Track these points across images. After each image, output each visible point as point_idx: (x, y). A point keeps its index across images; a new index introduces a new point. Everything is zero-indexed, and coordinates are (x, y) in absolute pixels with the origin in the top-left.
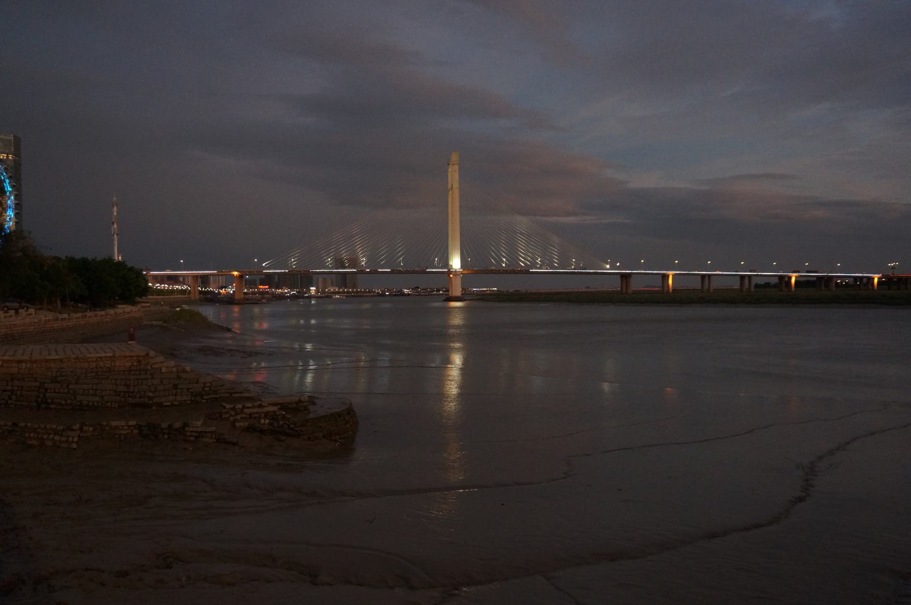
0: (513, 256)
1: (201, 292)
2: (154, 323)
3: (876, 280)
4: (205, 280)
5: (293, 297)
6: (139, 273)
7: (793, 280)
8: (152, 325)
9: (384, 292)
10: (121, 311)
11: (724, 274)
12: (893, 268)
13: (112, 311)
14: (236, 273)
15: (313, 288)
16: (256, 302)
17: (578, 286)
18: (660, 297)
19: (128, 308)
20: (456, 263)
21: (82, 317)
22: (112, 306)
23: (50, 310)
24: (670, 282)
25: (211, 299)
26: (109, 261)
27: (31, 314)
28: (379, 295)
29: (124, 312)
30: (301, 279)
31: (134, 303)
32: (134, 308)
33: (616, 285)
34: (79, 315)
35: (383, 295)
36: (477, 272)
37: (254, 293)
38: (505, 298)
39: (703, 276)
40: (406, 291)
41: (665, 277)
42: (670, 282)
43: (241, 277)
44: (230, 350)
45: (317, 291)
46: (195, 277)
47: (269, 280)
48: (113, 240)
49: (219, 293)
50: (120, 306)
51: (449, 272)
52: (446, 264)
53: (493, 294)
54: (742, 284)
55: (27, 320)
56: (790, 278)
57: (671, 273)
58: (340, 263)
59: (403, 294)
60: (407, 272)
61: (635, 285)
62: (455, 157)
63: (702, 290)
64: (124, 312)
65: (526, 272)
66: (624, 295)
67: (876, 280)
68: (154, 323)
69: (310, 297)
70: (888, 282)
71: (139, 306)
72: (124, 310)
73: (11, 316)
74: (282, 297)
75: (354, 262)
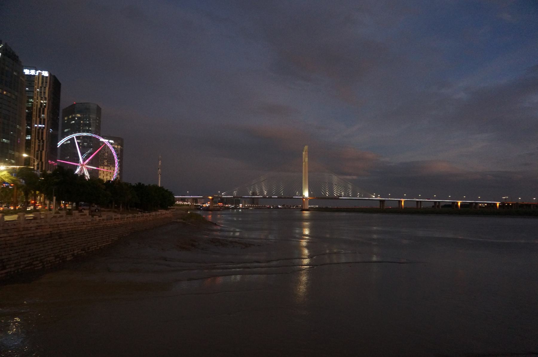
0: (331, 192)
1: (195, 206)
2: (178, 220)
3: (498, 205)
4: (196, 200)
5: (232, 208)
6: (171, 194)
7: (459, 204)
8: (177, 222)
9: (270, 207)
10: (159, 213)
11: (427, 201)
12: (505, 199)
13: (154, 213)
14: (210, 197)
15: (241, 205)
16: (218, 210)
17: (350, 206)
18: (398, 211)
19: (164, 212)
20: (306, 194)
21: (132, 217)
22: (155, 210)
23: (115, 212)
24: (403, 204)
25: (198, 208)
26: (156, 187)
27: (85, 215)
28: (268, 208)
29: (161, 214)
30: (236, 201)
31: (167, 209)
32: (167, 212)
33: (378, 206)
34: (130, 215)
35: (270, 208)
36: (318, 198)
37: (217, 206)
38: (326, 210)
39: (417, 202)
40: (279, 206)
41: (400, 202)
42: (403, 204)
43: (212, 199)
44: (231, 242)
45: (243, 206)
46: (193, 199)
47: (222, 200)
48: (158, 178)
49: (203, 206)
50: (160, 211)
51: (303, 198)
52: (301, 194)
53: (316, 208)
54: (417, 205)
55: (80, 220)
56: (457, 203)
57: (403, 200)
58: (254, 194)
59: (279, 208)
60: (285, 198)
61: (387, 206)
62: (306, 147)
63: (380, 208)
64: (161, 214)
65: (337, 198)
66: (382, 209)
67: (498, 205)
68: (178, 220)
69: (240, 208)
70: (502, 205)
71: (170, 210)
72: (162, 213)
73: (61, 216)
74: (228, 208)
75: (262, 193)
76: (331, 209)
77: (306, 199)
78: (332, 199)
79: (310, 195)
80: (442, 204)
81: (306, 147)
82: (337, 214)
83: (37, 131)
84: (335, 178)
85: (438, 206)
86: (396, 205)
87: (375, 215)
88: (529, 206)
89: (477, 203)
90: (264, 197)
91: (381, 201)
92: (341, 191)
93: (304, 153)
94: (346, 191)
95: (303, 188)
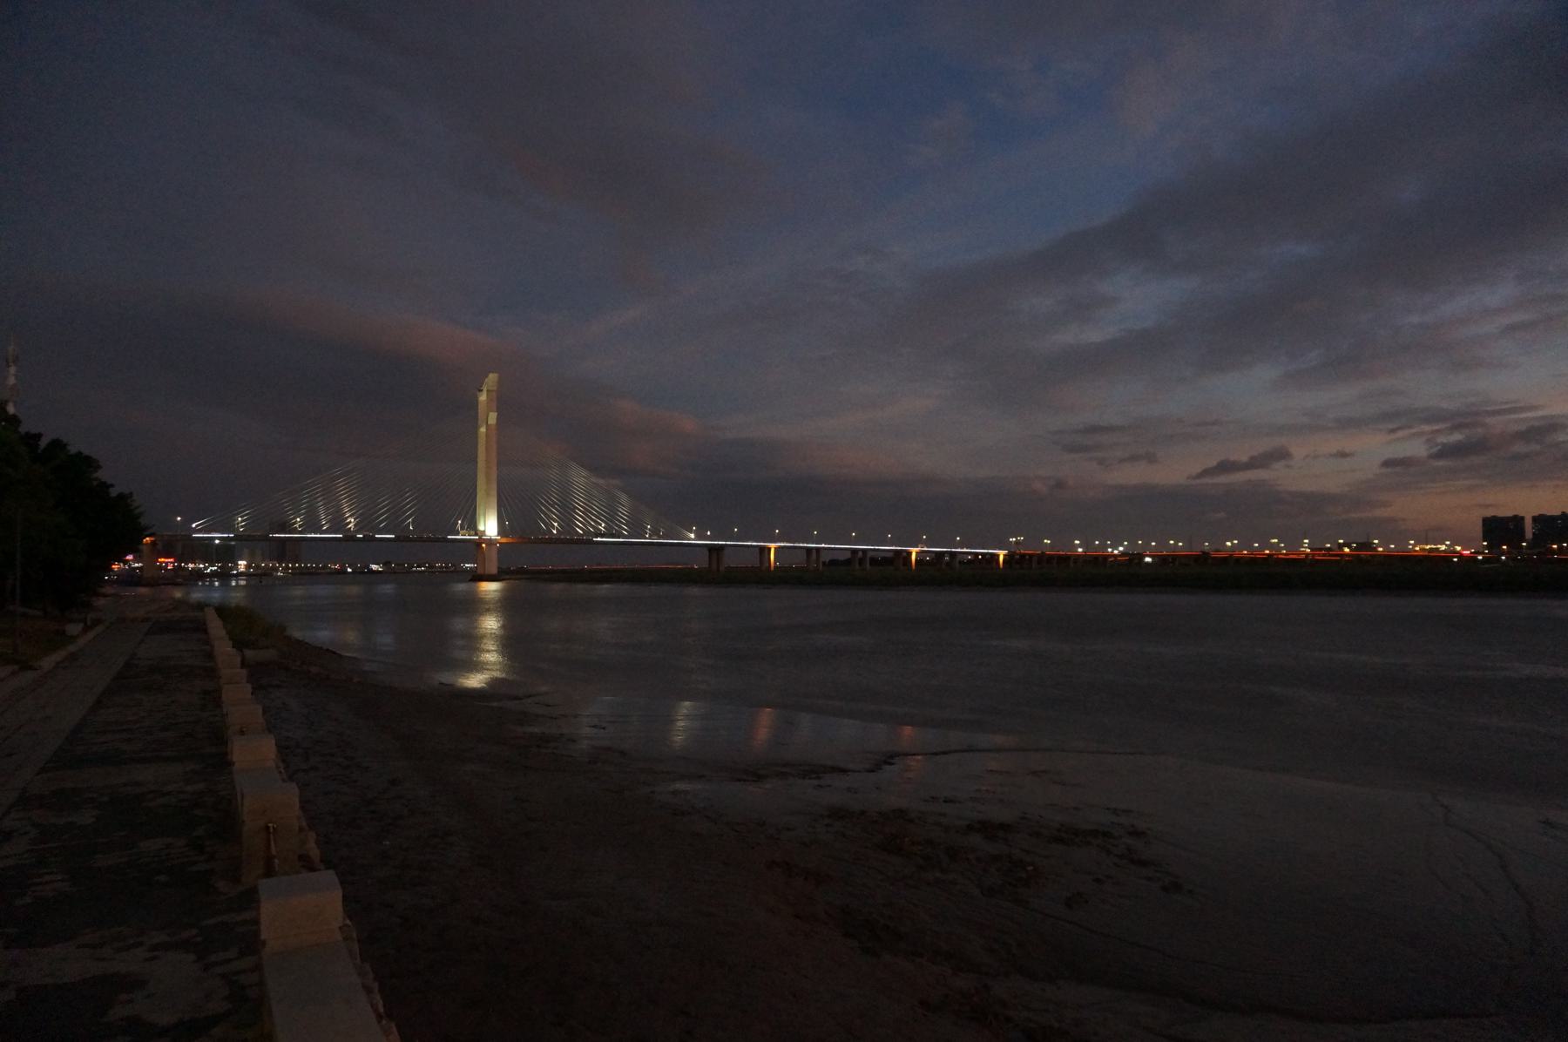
0: (567, 523)
5: (213, 574)
12: (1017, 543)
20: (489, 526)
28: (337, 572)
39: (809, 550)
40: (374, 567)
41: (764, 551)
45: (248, 567)
52: (472, 525)
57: (773, 546)
61: (729, 561)
62: (492, 378)
66: (716, 572)
74: (199, 575)
75: (338, 524)
76: (591, 572)
77: (490, 542)
78: (571, 541)
79: (502, 530)
80: (826, 558)
81: (492, 378)
82: (580, 588)
83: (1393, 436)
84: (580, 478)
85: (861, 561)
86: (754, 561)
87: (695, 591)
88: (1064, 560)
89: (953, 555)
90: (350, 538)
91: (711, 548)
92: (595, 517)
93: (483, 397)
94: (611, 518)
95: (480, 511)
